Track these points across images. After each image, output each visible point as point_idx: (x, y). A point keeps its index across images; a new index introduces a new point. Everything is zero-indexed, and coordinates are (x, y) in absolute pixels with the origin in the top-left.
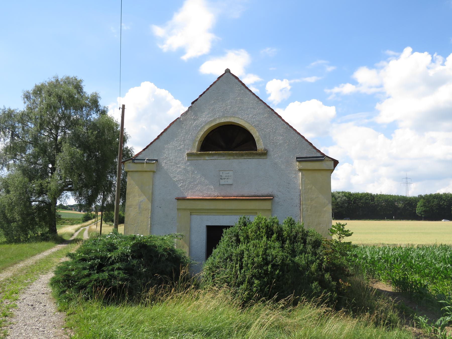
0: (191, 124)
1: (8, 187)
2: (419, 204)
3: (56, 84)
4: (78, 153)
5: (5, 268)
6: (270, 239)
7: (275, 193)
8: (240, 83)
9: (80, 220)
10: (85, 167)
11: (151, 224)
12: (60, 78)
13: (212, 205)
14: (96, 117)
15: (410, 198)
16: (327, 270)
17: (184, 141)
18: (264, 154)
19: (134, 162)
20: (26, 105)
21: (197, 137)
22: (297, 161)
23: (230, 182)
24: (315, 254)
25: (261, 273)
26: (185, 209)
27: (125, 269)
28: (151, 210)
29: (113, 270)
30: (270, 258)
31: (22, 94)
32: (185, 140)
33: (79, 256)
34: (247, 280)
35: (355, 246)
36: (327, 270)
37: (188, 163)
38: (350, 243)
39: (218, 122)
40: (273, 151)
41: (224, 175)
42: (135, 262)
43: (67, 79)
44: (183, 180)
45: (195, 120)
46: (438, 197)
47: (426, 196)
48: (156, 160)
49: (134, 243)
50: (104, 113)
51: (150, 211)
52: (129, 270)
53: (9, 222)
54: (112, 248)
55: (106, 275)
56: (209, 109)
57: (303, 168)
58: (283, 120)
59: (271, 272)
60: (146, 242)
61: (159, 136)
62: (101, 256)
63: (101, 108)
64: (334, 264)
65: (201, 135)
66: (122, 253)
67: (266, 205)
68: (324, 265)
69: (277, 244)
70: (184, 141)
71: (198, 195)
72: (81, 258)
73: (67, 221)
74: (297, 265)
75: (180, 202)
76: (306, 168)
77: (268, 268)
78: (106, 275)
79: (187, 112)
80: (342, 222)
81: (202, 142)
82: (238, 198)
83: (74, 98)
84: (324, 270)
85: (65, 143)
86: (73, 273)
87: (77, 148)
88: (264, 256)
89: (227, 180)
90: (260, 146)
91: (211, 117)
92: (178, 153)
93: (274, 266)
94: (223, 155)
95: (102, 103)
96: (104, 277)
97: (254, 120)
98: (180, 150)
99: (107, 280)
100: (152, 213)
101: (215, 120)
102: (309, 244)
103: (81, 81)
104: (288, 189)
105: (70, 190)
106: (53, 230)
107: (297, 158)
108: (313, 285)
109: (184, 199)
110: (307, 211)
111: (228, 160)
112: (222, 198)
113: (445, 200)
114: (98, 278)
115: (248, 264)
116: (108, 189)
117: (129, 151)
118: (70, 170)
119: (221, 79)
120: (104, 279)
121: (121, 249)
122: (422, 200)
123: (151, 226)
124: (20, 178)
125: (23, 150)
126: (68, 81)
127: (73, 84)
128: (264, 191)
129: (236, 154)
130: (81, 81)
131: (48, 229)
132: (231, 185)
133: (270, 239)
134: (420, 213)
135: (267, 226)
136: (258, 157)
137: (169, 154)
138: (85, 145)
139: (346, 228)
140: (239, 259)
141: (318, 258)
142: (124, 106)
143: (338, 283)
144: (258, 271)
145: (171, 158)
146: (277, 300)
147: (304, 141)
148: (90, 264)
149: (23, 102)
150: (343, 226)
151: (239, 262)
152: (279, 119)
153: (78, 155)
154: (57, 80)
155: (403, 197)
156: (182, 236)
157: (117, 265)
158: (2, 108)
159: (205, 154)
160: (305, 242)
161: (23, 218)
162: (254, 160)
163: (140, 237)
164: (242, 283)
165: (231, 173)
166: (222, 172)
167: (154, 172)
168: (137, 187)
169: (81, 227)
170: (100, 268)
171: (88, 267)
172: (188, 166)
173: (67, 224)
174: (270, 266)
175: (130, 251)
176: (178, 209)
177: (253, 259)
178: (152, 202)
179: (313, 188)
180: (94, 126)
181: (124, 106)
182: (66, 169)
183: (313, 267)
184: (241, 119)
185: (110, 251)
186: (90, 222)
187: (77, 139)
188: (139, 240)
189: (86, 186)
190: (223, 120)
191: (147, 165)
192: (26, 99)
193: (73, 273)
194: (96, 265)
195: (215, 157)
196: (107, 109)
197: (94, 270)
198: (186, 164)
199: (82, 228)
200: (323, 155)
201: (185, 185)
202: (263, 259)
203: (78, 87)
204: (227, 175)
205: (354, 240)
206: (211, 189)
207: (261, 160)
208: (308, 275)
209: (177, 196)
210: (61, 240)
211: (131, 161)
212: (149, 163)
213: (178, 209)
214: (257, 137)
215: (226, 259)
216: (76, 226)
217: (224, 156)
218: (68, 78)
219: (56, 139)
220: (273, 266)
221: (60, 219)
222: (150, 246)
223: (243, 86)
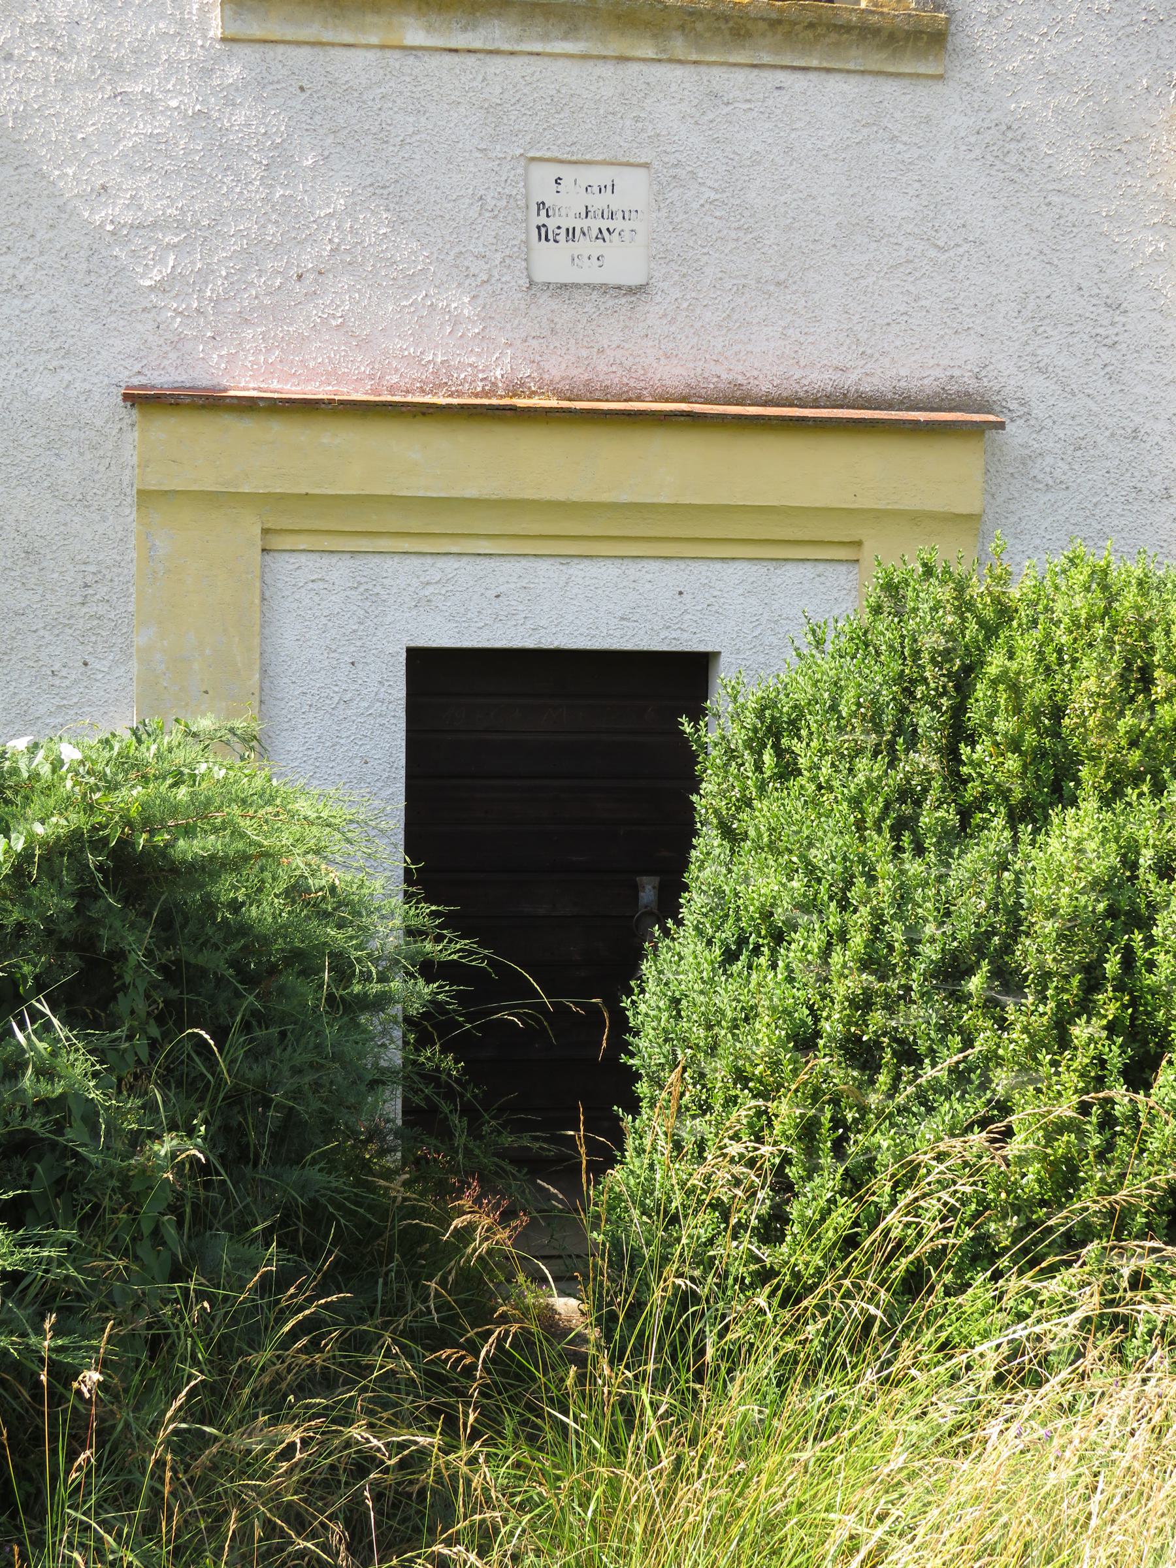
7: (1007, 376)
23: (623, 263)
37: (234, 72)
40: (991, 19)
41: (569, 205)
44: (181, 225)
75: (168, 430)
89: (597, 248)
104: (1106, 355)
109: (211, 403)
111: (606, 70)
112: (553, 403)
128: (909, 360)
131: (573, 1369)
132: (632, 291)
136: (876, 60)
162: (836, 85)
165: (633, 189)
176: (145, 497)
201: (206, 275)
204: (598, 202)
207: (888, 87)
213: (145, 497)
215: (951, 972)
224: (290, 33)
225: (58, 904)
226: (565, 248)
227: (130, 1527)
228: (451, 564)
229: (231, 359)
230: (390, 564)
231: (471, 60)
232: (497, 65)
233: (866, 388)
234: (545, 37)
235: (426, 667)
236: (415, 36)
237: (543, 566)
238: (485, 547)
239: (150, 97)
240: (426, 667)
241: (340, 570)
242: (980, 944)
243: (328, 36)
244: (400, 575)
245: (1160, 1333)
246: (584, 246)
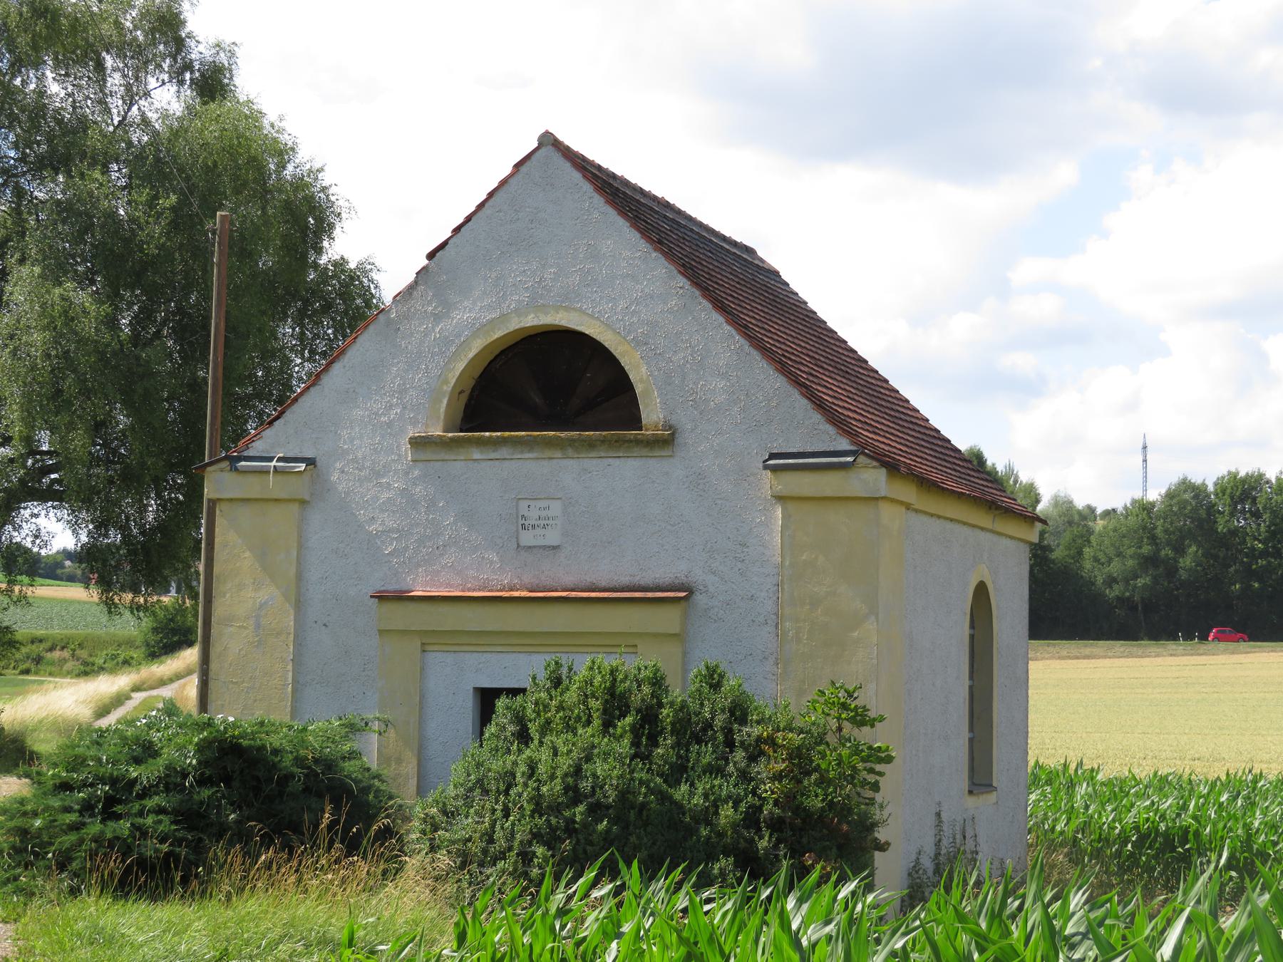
0: (426, 334)
4: (85, 312)
6: (611, 730)
7: (699, 576)
9: (130, 643)
10: (122, 372)
11: (295, 681)
14: (177, 108)
17: (402, 391)
19: (236, 470)
21: (446, 382)
23: (552, 537)
26: (404, 633)
27: (176, 812)
28: (296, 637)
29: (141, 814)
30: (586, 785)
32: (406, 390)
33: (53, 775)
34: (516, 844)
40: (693, 430)
41: (533, 515)
42: (206, 793)
44: (398, 531)
45: (437, 318)
48: (311, 462)
49: (204, 739)
50: (212, 83)
51: (292, 636)
54: (146, 751)
55: (123, 827)
57: (785, 493)
59: (585, 825)
62: (111, 774)
63: (200, 51)
65: (458, 374)
66: (168, 767)
67: (666, 619)
70: (402, 391)
71: (449, 585)
72: (58, 781)
73: (57, 654)
76: (796, 492)
77: (574, 814)
78: (123, 827)
79: (411, 288)
81: (464, 398)
82: (573, 594)
85: (22, 261)
86: (38, 823)
89: (542, 532)
90: (652, 412)
92: (383, 436)
93: (596, 810)
94: (529, 444)
96: (118, 833)
97: (635, 319)
98: (389, 424)
99: (125, 840)
101: (504, 318)
105: (44, 496)
109: (401, 597)
111: (545, 463)
114: (102, 832)
117: (353, 276)
119: (524, 169)
120: (117, 838)
121: (169, 754)
123: (294, 691)
128: (661, 571)
132: (554, 548)
133: (611, 730)
136: (645, 452)
137: (352, 440)
138: (115, 260)
140: (502, 787)
144: (548, 821)
145: (360, 455)
148: (84, 799)
153: (88, 327)
157: (150, 803)
163: (224, 721)
164: (502, 856)
165: (556, 508)
166: (527, 503)
167: (303, 502)
168: (247, 554)
169: (137, 688)
171: (77, 807)
173: (58, 670)
175: (194, 762)
176: (381, 632)
177: (538, 789)
178: (299, 605)
180: (156, 164)
184: (592, 316)
185: (137, 761)
188: (218, 731)
191: (279, 477)
193: (38, 823)
194: (99, 801)
195: (504, 452)
196: (232, 54)
197: (92, 815)
198: (407, 473)
199: (139, 697)
201: (406, 548)
202: (567, 789)
204: (543, 514)
206: (492, 562)
207: (652, 462)
208: (708, 838)
209: (378, 585)
211: (225, 464)
213: (381, 632)
214: (641, 381)
215: (471, 790)
216: (107, 685)
217: (531, 450)
222: (250, 747)
224: (434, 457)
227: (337, 810)
228: (489, 655)
229: (414, 580)
230: (467, 655)
231: (497, 463)
232: (507, 463)
233: (642, 583)
234: (522, 452)
236: (477, 455)
237: (522, 655)
238: (499, 649)
239: (388, 483)
243: (447, 457)
245: (7, 441)
246: (538, 531)
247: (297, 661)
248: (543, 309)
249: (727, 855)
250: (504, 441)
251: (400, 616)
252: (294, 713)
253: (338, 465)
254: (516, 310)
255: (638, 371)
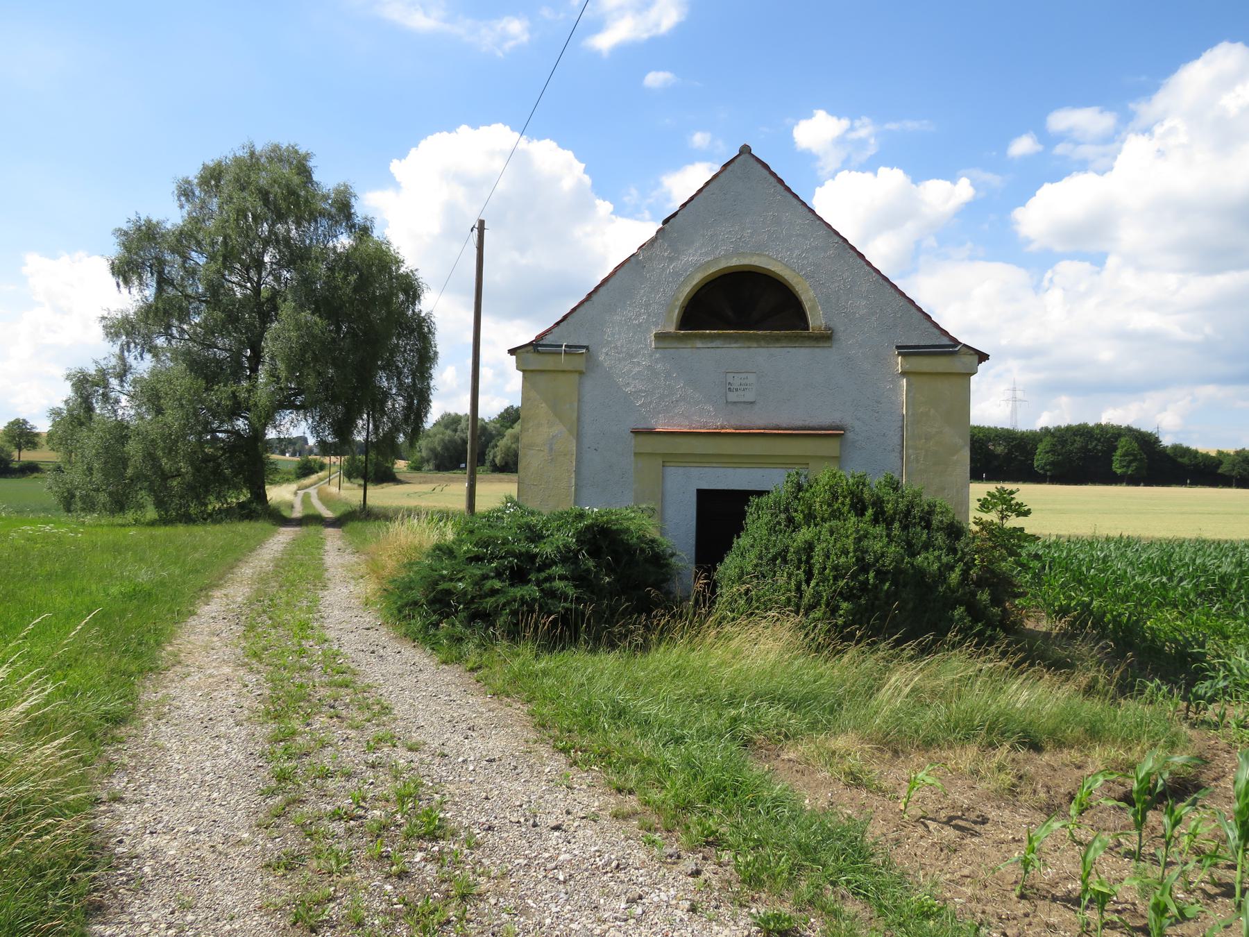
0: (664, 269)
1: (159, 398)
2: (1041, 447)
3: (251, 164)
5: (225, 574)
7: (848, 421)
8: (772, 179)
9: (289, 473)
11: (576, 485)
12: (258, 149)
13: (728, 447)
15: (1023, 433)
16: (980, 583)
17: (647, 305)
18: (826, 337)
20: (184, 212)
21: (678, 299)
22: (899, 354)
23: (749, 396)
24: (952, 550)
25: (853, 588)
29: (550, 579)
30: (869, 558)
31: (173, 187)
34: (823, 601)
35: (1034, 538)
36: (980, 583)
38: (1022, 529)
39: (723, 264)
41: (736, 383)
43: (273, 151)
45: (671, 260)
46: (1082, 432)
47: (1058, 429)
48: (587, 348)
50: (364, 232)
52: (581, 579)
53: (165, 477)
56: (703, 236)
57: (913, 370)
58: (869, 264)
59: (875, 586)
60: (608, 522)
61: (590, 295)
63: (358, 220)
64: (993, 572)
67: (830, 447)
68: (973, 573)
69: (879, 529)
70: (647, 305)
74: (920, 573)
79: (653, 241)
80: (1009, 486)
83: (299, 196)
84: (974, 583)
87: (313, 314)
88: (858, 553)
90: (816, 319)
91: (707, 254)
94: (735, 339)
95: (362, 208)
98: (640, 325)
100: (579, 462)
101: (716, 260)
102: (939, 529)
103: (306, 157)
106: (260, 496)
107: (898, 347)
108: (956, 613)
109: (651, 432)
110: (918, 461)
113: (1099, 440)
115: (825, 568)
116: (377, 402)
118: (298, 361)
119: (729, 168)
122: (1048, 438)
124: (185, 382)
125: (184, 316)
126: (277, 156)
127: (291, 163)
128: (824, 417)
129: (764, 338)
130: (306, 157)
134: (1043, 468)
135: (852, 493)
136: (813, 344)
137: (613, 335)
138: (327, 306)
139: (1018, 498)
140: (804, 558)
141: (961, 560)
142: (482, 223)
143: (1005, 610)
145: (619, 344)
146: (898, 643)
147: (914, 310)
149: (177, 204)
150: (1012, 493)
151: (803, 567)
152: (859, 260)
154: (252, 154)
155: (1008, 430)
156: (653, 510)
157: (557, 570)
158: (133, 218)
159: (696, 336)
160: (928, 526)
161: (198, 470)
165: (752, 378)
167: (581, 373)
170: (518, 576)
172: (657, 361)
174: (872, 574)
178: (579, 437)
179: (932, 411)
180: (346, 262)
181: (482, 223)
182: (288, 360)
183: (954, 577)
184: (776, 259)
186: (314, 477)
187: (309, 297)
189: (334, 399)
190: (735, 262)
191: (568, 357)
192: (183, 198)
200: (955, 342)
201: (651, 403)
203: (304, 171)
205: (1029, 525)
207: (817, 350)
210: (278, 518)
212: (570, 354)
215: (774, 559)
218: (276, 148)
219: (257, 290)
220: (879, 573)
221: (276, 471)
223: (779, 186)
225: (589, 536)
226: (735, 393)
235: (702, 494)
240: (702, 494)
241: (681, 470)
242: (779, 554)
244: (695, 472)
247: (578, 472)
248: (743, 254)
249: (961, 605)
250: (719, 336)
251: (649, 444)
252: (576, 503)
253: (604, 350)
254: (724, 256)
255: (807, 294)
